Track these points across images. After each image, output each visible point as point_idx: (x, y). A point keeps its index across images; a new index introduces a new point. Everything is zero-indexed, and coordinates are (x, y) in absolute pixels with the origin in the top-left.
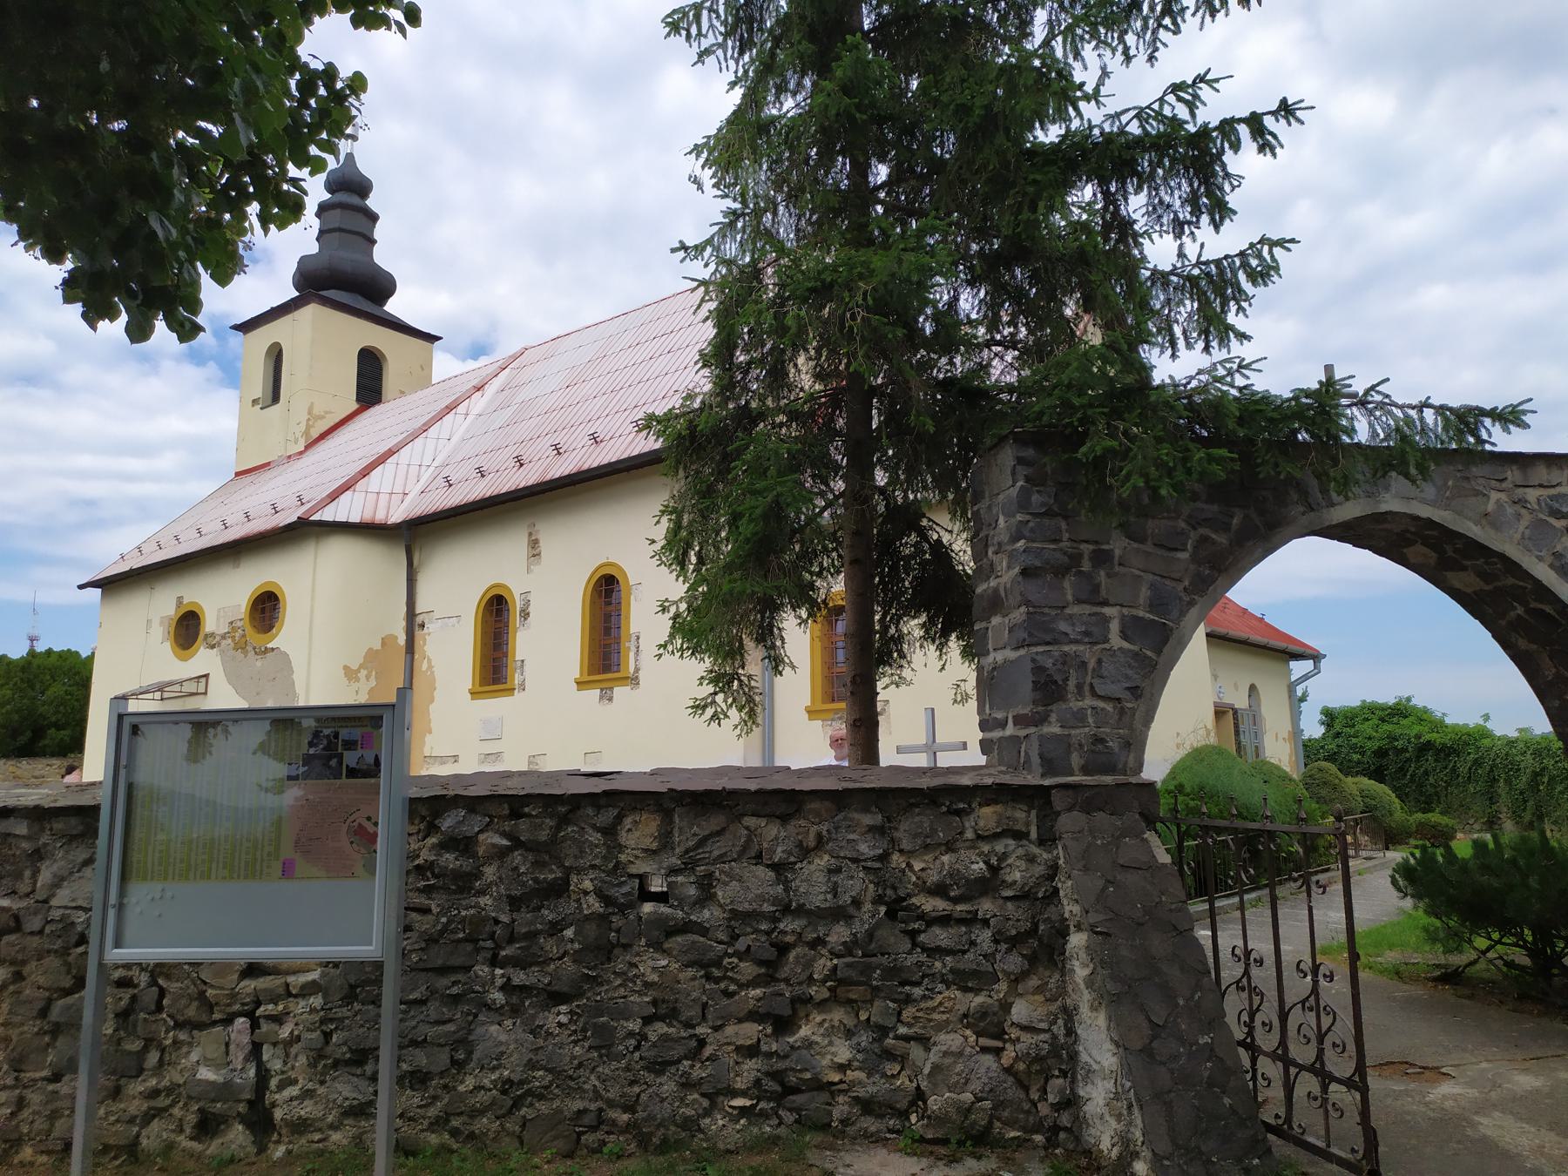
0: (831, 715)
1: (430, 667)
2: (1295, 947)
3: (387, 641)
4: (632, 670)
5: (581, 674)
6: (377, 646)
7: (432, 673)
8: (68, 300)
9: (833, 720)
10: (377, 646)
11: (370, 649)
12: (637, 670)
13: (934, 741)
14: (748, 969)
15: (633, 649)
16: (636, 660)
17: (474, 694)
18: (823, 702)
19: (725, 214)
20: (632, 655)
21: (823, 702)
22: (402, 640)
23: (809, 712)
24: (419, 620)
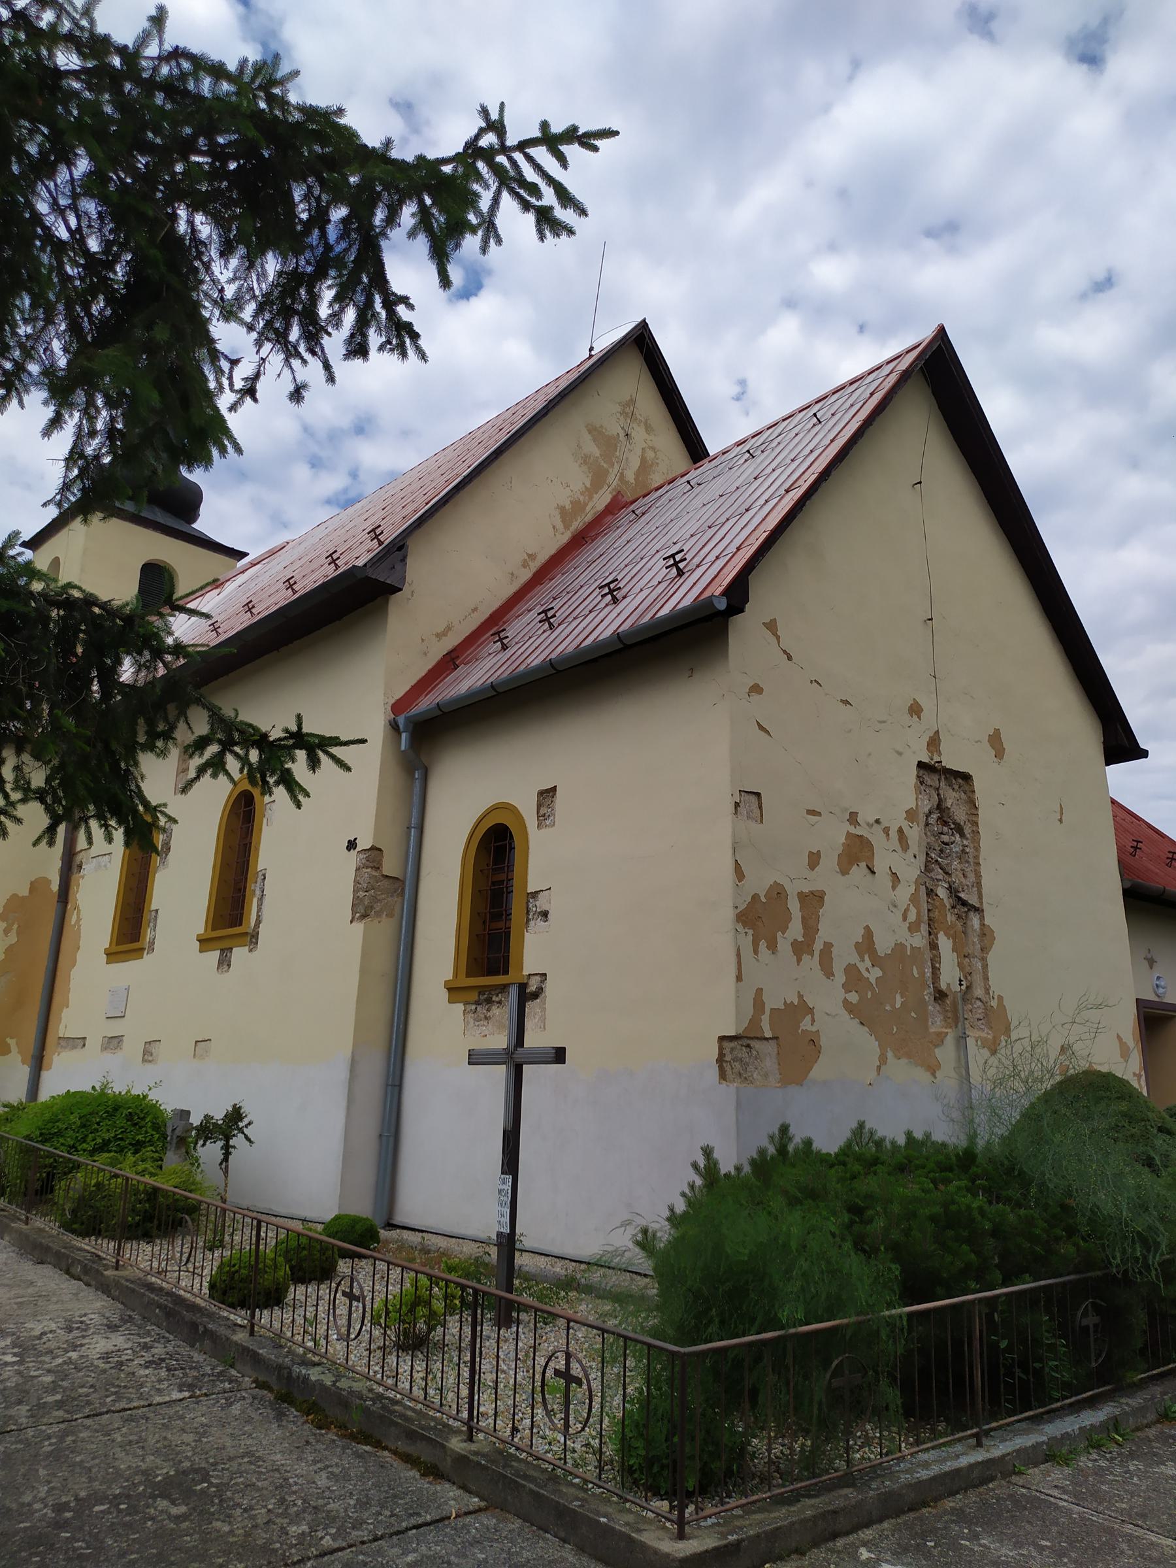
0: (474, 996)
1: (79, 919)
2: (276, 1325)
3: (38, 886)
4: (253, 924)
5: (206, 930)
6: (24, 891)
7: (79, 929)
8: (558, 236)
9: (477, 1003)
10: (24, 891)
11: (14, 896)
12: (258, 921)
13: (520, 1041)
14: (148, 1385)
15: (258, 893)
16: (259, 909)
17: (201, 951)
18: (468, 975)
19: (207, 462)
20: (255, 900)
21: (468, 975)
22: (55, 887)
23: (450, 990)
24: (78, 858)
